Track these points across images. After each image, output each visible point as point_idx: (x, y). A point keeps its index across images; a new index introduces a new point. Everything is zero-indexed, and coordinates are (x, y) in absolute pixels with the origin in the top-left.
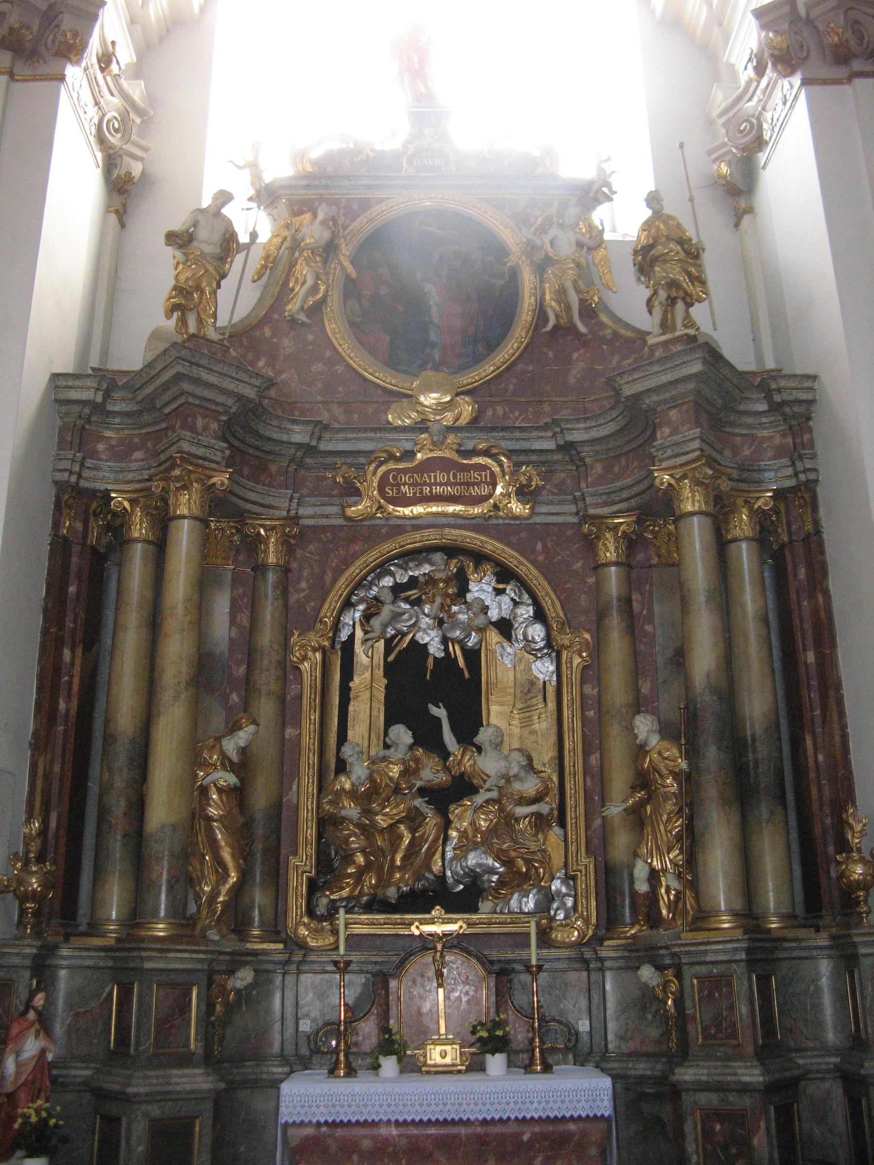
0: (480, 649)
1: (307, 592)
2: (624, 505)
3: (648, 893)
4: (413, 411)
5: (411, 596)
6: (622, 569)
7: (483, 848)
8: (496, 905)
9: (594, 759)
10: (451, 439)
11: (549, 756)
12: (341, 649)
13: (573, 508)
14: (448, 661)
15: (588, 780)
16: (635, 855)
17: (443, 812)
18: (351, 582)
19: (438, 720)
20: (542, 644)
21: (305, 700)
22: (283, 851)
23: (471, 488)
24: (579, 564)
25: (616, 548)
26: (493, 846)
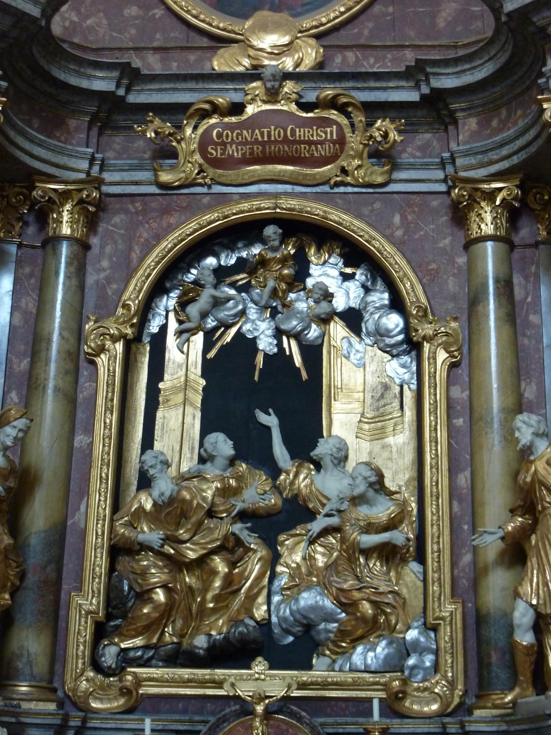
0: (322, 345)
1: (108, 272)
2: (505, 165)
3: (532, 646)
4: (244, 56)
5: (238, 281)
6: (500, 244)
7: (318, 588)
8: (334, 661)
9: (463, 479)
10: (289, 87)
11: (407, 476)
12: (150, 343)
13: (440, 175)
14: (281, 358)
15: (455, 504)
16: (516, 595)
17: (271, 544)
18: (163, 259)
19: (268, 429)
20: (401, 337)
21: (100, 401)
22: (65, 587)
23: (313, 147)
24: (447, 241)
25: (495, 218)
26: (331, 586)
